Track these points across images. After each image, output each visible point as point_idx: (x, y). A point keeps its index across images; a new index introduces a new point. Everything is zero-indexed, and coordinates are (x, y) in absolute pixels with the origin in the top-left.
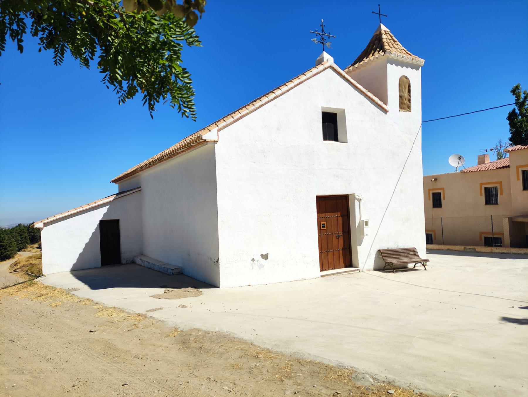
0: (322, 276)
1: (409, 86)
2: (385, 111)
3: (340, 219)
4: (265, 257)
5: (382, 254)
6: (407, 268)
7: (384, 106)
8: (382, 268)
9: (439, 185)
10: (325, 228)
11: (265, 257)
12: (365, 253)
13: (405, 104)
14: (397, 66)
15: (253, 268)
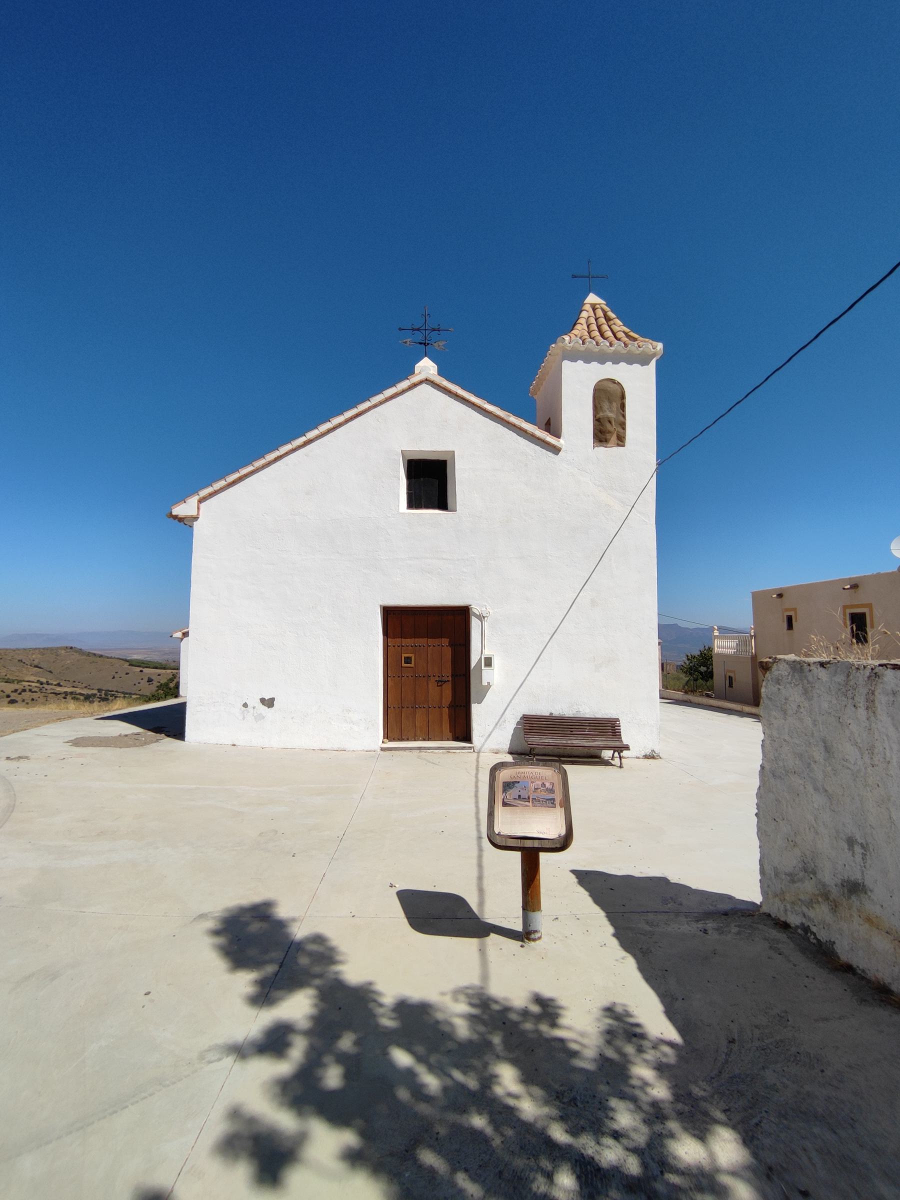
0: (382, 749)
1: (623, 397)
2: (556, 450)
3: (448, 652)
4: (269, 703)
5: (531, 724)
6: (599, 757)
7: (550, 439)
8: (528, 752)
9: (861, 599)
10: (412, 665)
11: (269, 703)
12: (494, 723)
13: (608, 429)
14: (587, 361)
15: (244, 718)
